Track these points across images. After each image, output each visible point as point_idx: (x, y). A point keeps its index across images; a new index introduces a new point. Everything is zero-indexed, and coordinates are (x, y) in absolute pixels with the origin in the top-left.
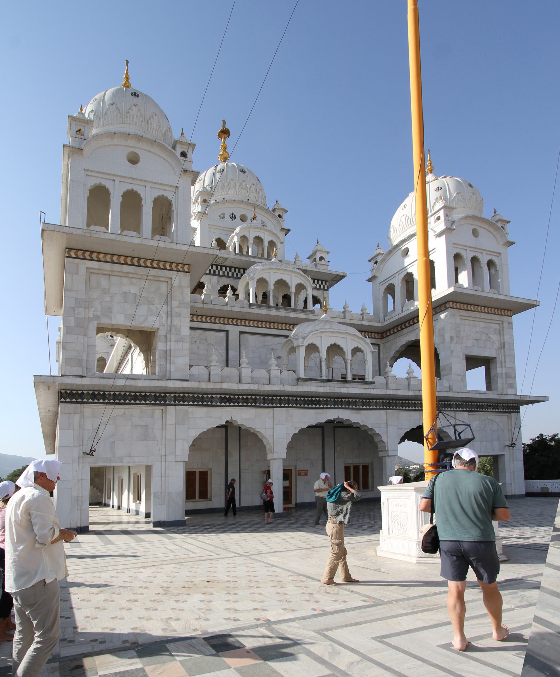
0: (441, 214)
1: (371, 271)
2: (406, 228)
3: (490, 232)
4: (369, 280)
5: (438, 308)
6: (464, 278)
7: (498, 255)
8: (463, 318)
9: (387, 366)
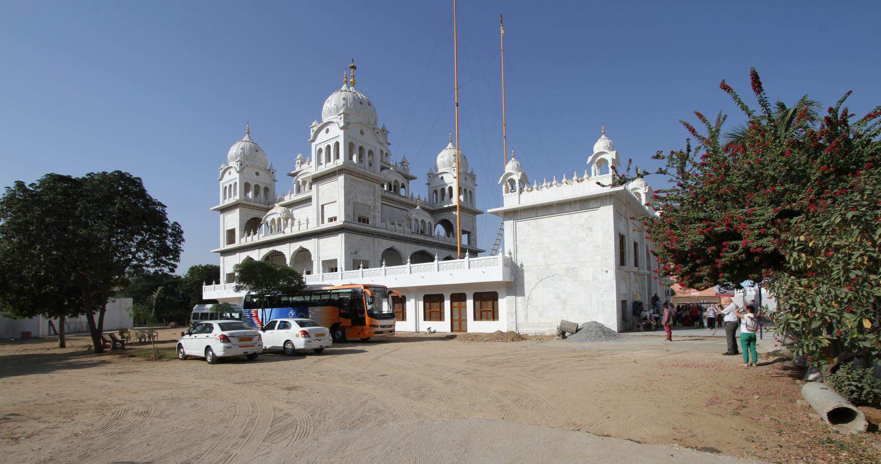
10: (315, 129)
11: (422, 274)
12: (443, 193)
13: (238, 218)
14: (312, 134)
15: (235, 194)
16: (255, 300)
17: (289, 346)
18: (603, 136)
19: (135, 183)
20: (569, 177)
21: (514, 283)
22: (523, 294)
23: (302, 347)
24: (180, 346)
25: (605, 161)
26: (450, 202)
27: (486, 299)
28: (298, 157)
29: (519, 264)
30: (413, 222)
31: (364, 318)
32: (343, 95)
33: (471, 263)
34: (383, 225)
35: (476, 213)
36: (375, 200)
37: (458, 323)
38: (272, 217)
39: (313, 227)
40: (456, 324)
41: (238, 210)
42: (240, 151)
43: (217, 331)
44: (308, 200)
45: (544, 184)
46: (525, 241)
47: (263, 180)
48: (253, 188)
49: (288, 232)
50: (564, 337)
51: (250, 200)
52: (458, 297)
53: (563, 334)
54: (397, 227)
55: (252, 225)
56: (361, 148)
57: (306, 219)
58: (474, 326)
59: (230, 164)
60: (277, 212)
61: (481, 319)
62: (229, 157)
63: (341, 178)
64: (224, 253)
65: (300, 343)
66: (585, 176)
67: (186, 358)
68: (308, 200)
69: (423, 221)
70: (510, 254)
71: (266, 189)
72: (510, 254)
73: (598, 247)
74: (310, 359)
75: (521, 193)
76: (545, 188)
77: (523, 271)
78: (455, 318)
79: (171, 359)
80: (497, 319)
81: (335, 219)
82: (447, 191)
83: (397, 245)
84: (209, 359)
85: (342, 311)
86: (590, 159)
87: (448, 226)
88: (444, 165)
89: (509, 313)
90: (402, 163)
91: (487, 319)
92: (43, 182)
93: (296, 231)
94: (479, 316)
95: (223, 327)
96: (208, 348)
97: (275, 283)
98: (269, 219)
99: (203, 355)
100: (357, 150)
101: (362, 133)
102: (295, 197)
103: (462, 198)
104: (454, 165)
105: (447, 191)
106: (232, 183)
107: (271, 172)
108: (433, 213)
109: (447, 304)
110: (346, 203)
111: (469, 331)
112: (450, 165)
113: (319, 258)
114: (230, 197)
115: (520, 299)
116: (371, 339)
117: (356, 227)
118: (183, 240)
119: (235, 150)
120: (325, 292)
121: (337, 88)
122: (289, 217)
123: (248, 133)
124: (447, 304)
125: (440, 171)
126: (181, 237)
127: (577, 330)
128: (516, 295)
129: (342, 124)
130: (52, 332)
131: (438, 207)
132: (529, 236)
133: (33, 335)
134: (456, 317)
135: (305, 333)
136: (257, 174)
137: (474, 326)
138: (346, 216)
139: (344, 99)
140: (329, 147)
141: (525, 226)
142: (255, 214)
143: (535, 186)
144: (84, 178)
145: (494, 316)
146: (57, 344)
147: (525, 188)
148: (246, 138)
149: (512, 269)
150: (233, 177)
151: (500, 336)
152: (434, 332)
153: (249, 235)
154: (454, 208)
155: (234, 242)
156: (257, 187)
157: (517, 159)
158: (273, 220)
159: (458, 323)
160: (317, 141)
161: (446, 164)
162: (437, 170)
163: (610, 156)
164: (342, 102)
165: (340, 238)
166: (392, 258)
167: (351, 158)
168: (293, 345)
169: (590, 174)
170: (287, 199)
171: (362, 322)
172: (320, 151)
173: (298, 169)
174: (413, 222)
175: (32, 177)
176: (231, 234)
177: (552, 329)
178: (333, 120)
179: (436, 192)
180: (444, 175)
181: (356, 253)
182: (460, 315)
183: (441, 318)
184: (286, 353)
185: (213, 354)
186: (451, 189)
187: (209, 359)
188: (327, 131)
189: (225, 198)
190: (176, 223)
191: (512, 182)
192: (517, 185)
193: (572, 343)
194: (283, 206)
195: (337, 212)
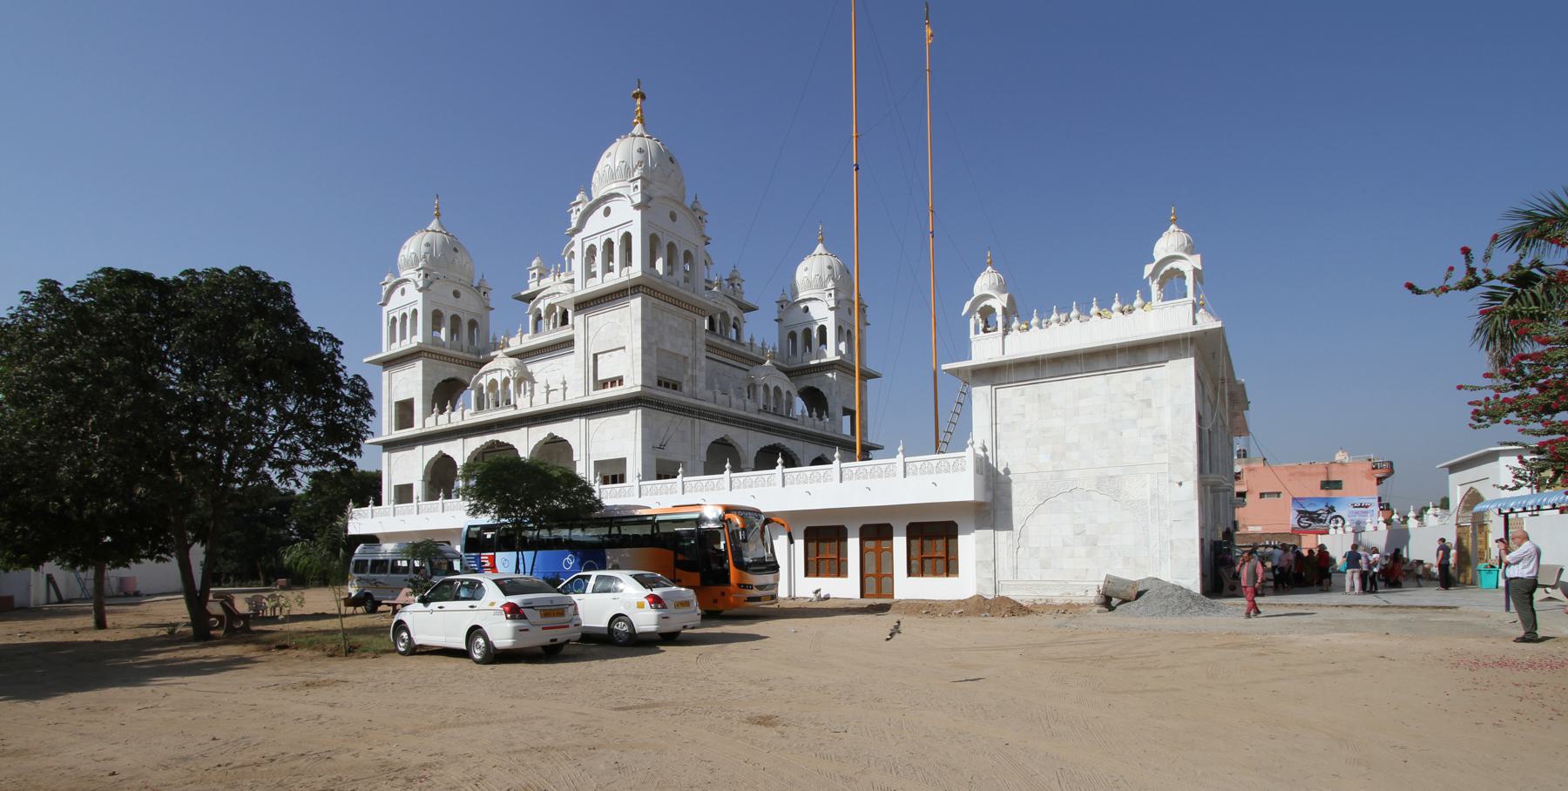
10: (582, 207)
11: (809, 487)
12: (809, 337)
13: (420, 378)
14: (574, 220)
15: (414, 333)
16: (489, 536)
17: (621, 627)
18: (1173, 227)
19: (279, 293)
20: (1106, 305)
21: (992, 507)
22: (1007, 525)
23: (652, 628)
24: (401, 626)
25: (1180, 275)
26: (821, 354)
27: (934, 537)
28: (534, 263)
29: (1001, 470)
30: (761, 391)
31: (728, 571)
32: (638, 143)
33: (787, 477)
34: (709, 394)
36: (694, 347)
37: (876, 579)
38: (490, 377)
39: (576, 396)
40: (871, 582)
41: (419, 364)
42: (424, 249)
43: (493, 595)
44: (568, 343)
45: (1054, 317)
46: (1009, 423)
47: (467, 306)
48: (448, 321)
49: (524, 406)
50: (1112, 609)
51: (443, 345)
52: (876, 531)
53: (1107, 602)
54: (719, 396)
55: (445, 393)
56: (671, 247)
57: (561, 381)
58: (907, 587)
59: (404, 275)
60: (500, 367)
61: (922, 573)
62: (401, 260)
63: (636, 303)
64: (390, 446)
65: (646, 620)
66: (1138, 302)
67: (415, 650)
68: (568, 343)
69: (777, 389)
70: (984, 449)
71: (473, 324)
72: (984, 449)
73: (1163, 436)
74: (671, 653)
75: (1005, 333)
76: (1055, 325)
77: (1010, 481)
78: (867, 572)
79: (378, 654)
80: (956, 573)
81: (621, 380)
82: (815, 334)
83: (735, 434)
84: (477, 654)
85: (680, 557)
86: (1148, 269)
87: (815, 399)
89: (978, 558)
90: (731, 280)
91: (935, 574)
92: (91, 287)
93: (540, 404)
94: (917, 567)
95: (506, 587)
96: (474, 632)
97: (536, 503)
98: (484, 381)
99: (464, 647)
100: (665, 250)
101: (673, 217)
102: (529, 341)
103: (842, 347)
104: (830, 285)
105: (815, 334)
106: (409, 312)
107: (481, 290)
108: (790, 373)
109: (853, 545)
110: (646, 350)
111: (897, 596)
112: (822, 285)
113: (588, 456)
114: (403, 337)
115: (1002, 535)
116: (726, 612)
117: (657, 399)
118: (373, 412)
119: (413, 247)
120: (641, 521)
121: (625, 131)
122: (525, 378)
123: (438, 215)
124: (853, 545)
125: (802, 296)
126: (368, 405)
127: (1139, 594)
128: (994, 527)
129: (638, 199)
130: (54, 597)
131: (797, 363)
132: (1023, 415)
133: (18, 601)
134: (871, 569)
135: (656, 601)
136: (456, 294)
137: (907, 587)
138: (645, 375)
139: (640, 151)
140: (609, 243)
141: (1010, 395)
142: (452, 371)
143: (1034, 321)
144: (176, 280)
145: (949, 567)
146: (90, 621)
147: (1015, 324)
148: (434, 224)
149: (987, 479)
150: (409, 299)
151: (980, 607)
152: (827, 598)
153: (442, 411)
154: (830, 366)
155: (412, 426)
156: (456, 320)
157: (997, 269)
158: (493, 383)
159: (876, 579)
160: (585, 232)
161: (813, 279)
162: (795, 293)
163: (1189, 265)
164: (637, 157)
165: (634, 418)
166: (720, 457)
167: (653, 265)
168: (630, 624)
169: (1147, 298)
170: (515, 344)
171: (724, 578)
172: (592, 251)
173: (533, 287)
174: (761, 391)
175: (72, 274)
176: (404, 411)
177: (1087, 590)
178: (620, 191)
179: (793, 336)
180: (809, 304)
181: (662, 447)
182: (879, 569)
183: (840, 570)
184: (617, 640)
185: (488, 643)
186: (823, 329)
187: (477, 654)
188: (607, 212)
189: (393, 340)
190: (358, 377)
191: (987, 313)
192: (999, 319)
193: (1121, 618)
194: (511, 355)
195: (628, 369)
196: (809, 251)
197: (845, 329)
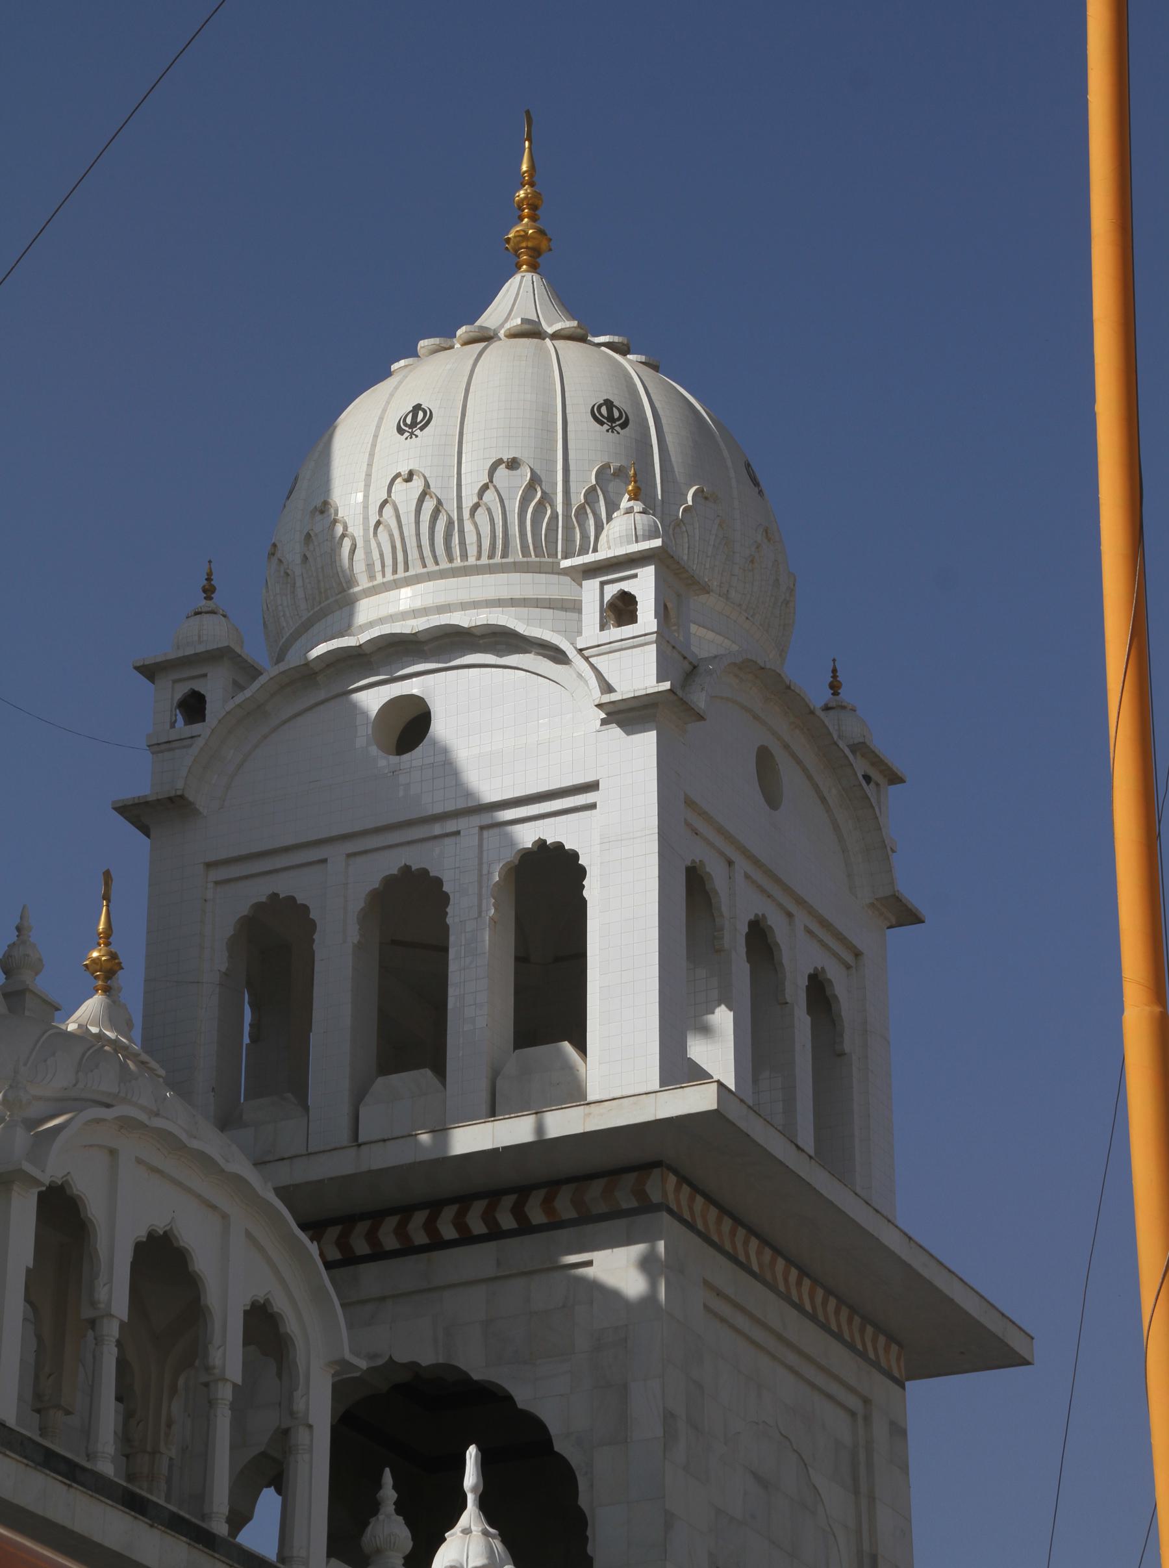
0: (643, 585)
1: (159, 747)
2: (416, 569)
3: (823, 800)
4: (140, 814)
5: (597, 1186)
6: (717, 1052)
7: (849, 958)
8: (725, 1310)
9: (374, 1508)
35: (936, 1333)
69: (160, 1258)
88: (440, 536)
99: (485, 833)
104: (622, 531)
112: (544, 533)
137: (628, 1061)
139: (609, 415)
154: (617, 1179)
162: (334, 597)
179: (273, 951)
186: (550, 888)
196: (447, 309)
197: (739, 904)
